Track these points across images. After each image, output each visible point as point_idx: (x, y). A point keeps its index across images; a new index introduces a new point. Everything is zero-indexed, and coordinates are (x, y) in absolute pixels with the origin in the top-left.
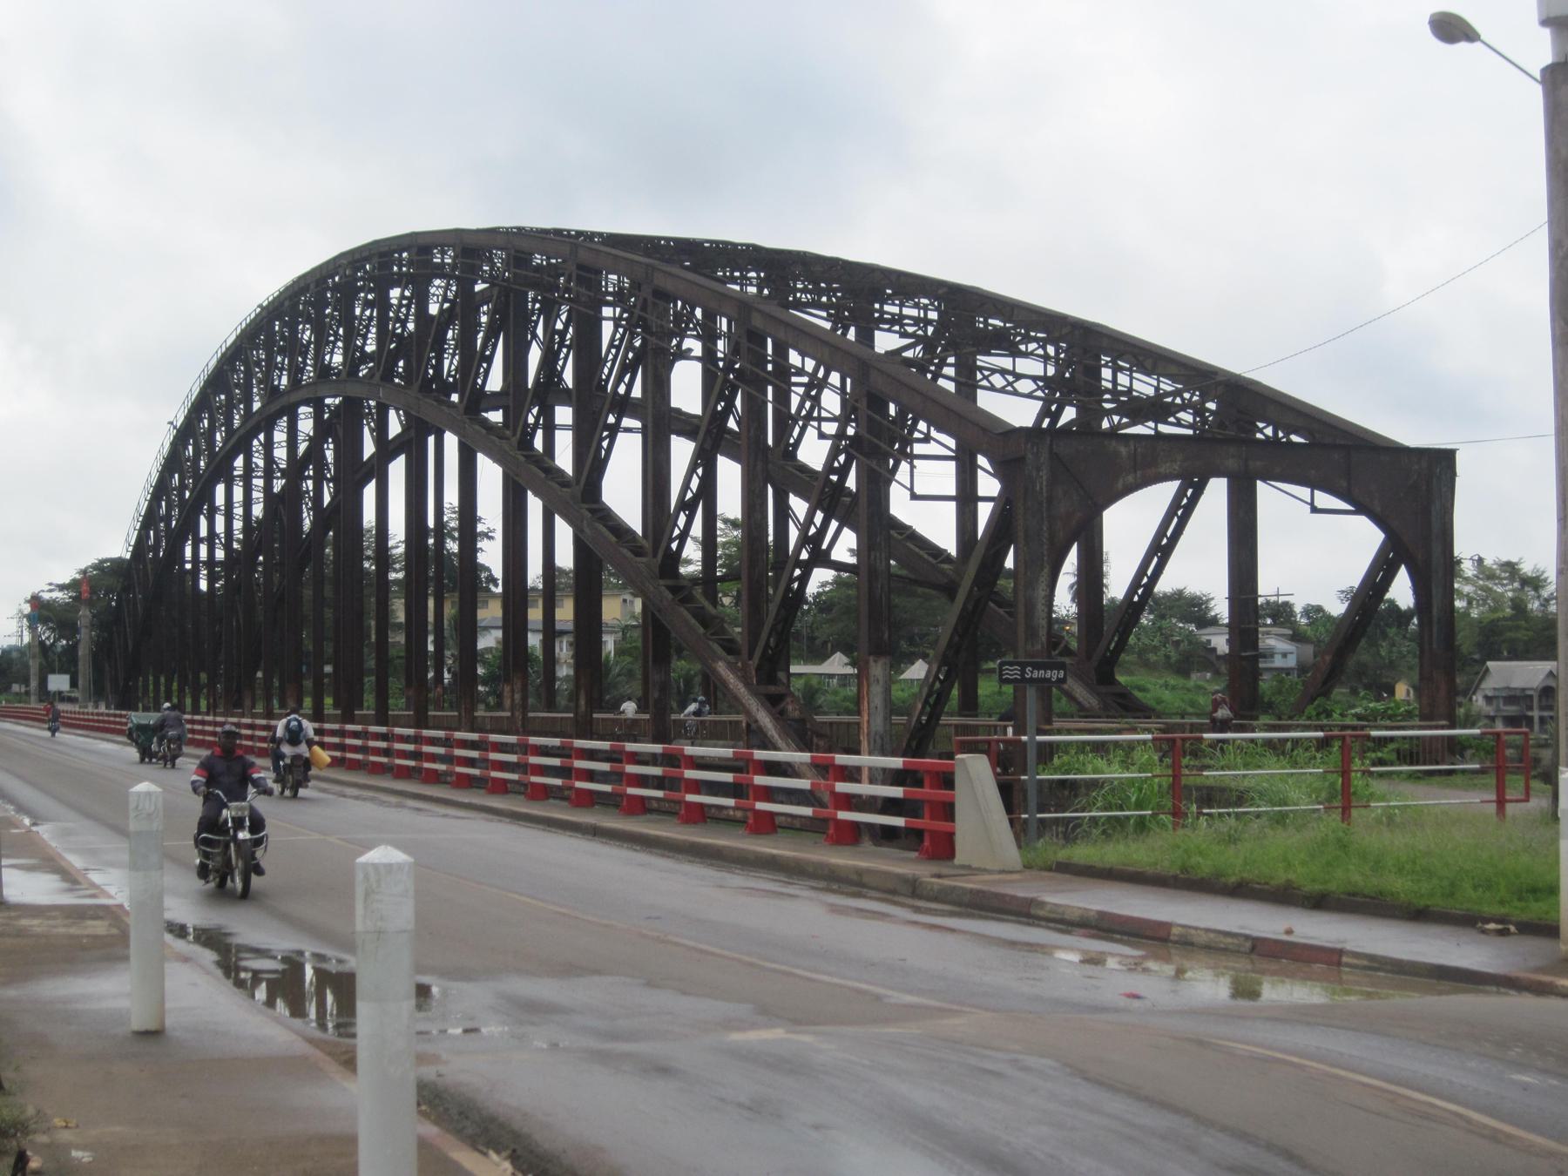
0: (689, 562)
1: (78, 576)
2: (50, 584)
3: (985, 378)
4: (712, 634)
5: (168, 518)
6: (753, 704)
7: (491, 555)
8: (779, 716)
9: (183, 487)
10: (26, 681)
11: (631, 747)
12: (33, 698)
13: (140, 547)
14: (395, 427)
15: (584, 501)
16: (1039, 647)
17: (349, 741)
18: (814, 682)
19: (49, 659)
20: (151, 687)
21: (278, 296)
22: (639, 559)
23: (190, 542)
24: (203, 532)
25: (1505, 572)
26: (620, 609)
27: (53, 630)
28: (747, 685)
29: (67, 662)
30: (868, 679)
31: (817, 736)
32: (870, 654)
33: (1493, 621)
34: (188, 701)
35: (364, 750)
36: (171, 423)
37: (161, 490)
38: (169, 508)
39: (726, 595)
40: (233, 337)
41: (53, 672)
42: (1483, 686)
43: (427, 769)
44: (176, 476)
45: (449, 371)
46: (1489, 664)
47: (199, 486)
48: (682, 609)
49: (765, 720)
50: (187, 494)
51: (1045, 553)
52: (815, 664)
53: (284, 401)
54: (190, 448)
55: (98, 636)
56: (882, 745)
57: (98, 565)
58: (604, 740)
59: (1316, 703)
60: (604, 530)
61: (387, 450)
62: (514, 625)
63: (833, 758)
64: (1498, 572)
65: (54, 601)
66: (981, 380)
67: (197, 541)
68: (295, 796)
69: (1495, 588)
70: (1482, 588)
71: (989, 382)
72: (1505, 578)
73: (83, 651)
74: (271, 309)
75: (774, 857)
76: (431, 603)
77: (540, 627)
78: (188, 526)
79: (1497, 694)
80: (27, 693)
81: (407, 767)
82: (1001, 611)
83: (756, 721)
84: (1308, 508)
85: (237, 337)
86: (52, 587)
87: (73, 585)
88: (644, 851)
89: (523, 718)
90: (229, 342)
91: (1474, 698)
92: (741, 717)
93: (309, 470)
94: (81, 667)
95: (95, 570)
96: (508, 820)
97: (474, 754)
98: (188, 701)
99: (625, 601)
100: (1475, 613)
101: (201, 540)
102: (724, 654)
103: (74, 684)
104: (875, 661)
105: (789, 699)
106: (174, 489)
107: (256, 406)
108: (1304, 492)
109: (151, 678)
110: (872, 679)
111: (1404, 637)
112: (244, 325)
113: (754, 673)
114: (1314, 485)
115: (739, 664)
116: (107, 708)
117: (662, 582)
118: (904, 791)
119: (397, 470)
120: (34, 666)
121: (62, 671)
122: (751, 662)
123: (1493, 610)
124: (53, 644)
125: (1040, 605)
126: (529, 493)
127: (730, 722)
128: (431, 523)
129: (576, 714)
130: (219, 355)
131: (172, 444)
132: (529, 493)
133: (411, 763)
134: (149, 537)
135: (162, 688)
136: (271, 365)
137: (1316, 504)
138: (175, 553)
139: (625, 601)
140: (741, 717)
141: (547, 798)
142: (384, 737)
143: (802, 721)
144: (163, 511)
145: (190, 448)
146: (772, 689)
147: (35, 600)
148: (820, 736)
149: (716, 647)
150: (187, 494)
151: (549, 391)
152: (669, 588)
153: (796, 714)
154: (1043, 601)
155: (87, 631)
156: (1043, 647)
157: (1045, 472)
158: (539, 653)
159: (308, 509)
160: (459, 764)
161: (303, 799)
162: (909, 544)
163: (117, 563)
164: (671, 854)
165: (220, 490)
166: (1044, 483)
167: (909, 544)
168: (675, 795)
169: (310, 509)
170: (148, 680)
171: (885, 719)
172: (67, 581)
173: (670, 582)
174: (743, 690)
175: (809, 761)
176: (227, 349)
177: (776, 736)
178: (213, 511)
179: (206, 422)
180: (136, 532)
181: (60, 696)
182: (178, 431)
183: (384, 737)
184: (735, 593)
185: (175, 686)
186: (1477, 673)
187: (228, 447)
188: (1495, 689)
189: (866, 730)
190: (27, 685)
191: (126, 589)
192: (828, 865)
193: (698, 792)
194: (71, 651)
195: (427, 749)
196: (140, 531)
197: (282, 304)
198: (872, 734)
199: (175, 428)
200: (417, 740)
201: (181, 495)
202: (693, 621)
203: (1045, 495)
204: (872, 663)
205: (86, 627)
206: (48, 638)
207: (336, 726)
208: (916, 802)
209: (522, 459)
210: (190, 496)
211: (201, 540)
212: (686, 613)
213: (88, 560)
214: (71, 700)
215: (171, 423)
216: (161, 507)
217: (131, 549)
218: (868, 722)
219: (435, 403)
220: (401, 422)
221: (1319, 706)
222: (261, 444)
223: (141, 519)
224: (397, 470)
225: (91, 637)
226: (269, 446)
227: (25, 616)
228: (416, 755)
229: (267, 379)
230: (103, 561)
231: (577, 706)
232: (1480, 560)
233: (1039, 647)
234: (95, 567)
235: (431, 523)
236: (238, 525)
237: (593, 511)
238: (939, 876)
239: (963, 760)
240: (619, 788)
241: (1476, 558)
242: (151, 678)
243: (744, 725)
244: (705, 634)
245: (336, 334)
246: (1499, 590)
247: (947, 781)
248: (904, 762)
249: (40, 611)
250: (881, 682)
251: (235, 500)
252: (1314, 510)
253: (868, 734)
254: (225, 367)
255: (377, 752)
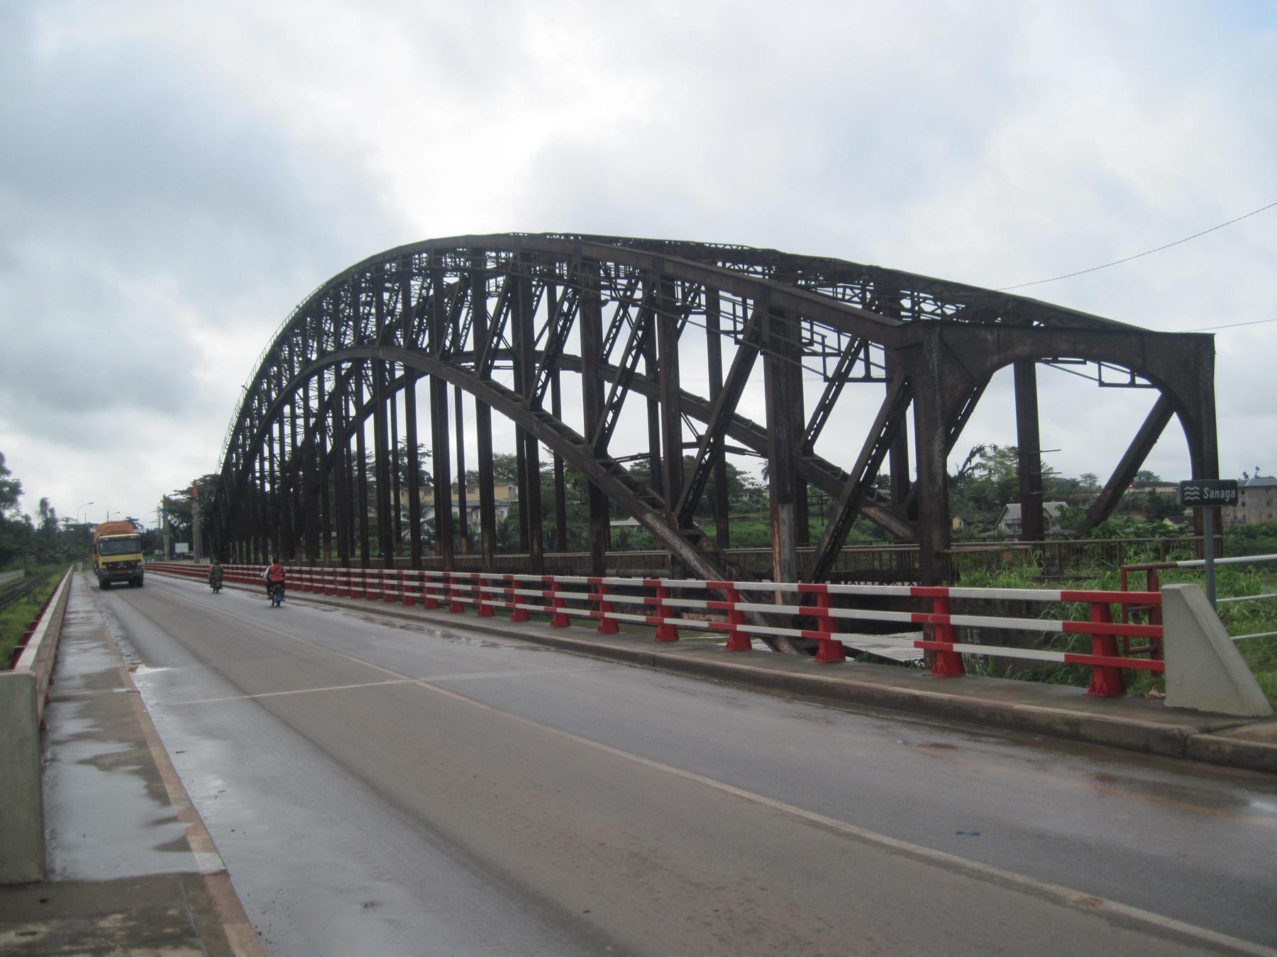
0: (545, 464)
1: (191, 486)
2: (175, 491)
3: (856, 295)
4: (640, 495)
5: (243, 446)
6: (677, 543)
7: (428, 466)
8: (700, 552)
9: (252, 426)
10: (162, 548)
11: (483, 575)
12: (166, 558)
13: (227, 465)
14: (367, 397)
15: (531, 410)
16: (937, 490)
17: (315, 577)
18: (626, 530)
19: (174, 534)
20: (237, 548)
21: (309, 301)
22: (578, 446)
23: (258, 460)
24: (266, 454)
25: (1012, 453)
26: (505, 494)
27: (178, 517)
28: (672, 528)
29: (186, 536)
30: (778, 521)
31: (729, 564)
32: (779, 502)
33: (1006, 481)
34: (261, 557)
35: (311, 580)
36: (244, 386)
37: (239, 429)
38: (244, 439)
39: (567, 483)
40: (281, 329)
41: (178, 542)
42: (1005, 518)
43: (354, 591)
44: (248, 420)
45: (424, 334)
46: (1007, 505)
47: (263, 424)
48: (615, 479)
49: (687, 553)
50: (255, 430)
51: (939, 416)
52: (622, 520)
53: (315, 366)
54: (256, 402)
55: (205, 520)
56: (790, 569)
57: (204, 479)
58: (499, 573)
59: (1100, 526)
60: (549, 428)
61: (363, 412)
62: (442, 504)
63: (601, 580)
64: (1008, 453)
65: (178, 500)
66: (859, 293)
67: (262, 460)
68: (278, 605)
69: (1006, 462)
70: (999, 463)
71: (854, 292)
72: (1012, 457)
73: (195, 529)
74: (305, 308)
75: (916, 698)
76: (392, 495)
77: (458, 504)
78: (257, 449)
79: (1014, 522)
80: (163, 555)
81: (393, 595)
82: (828, 473)
83: (681, 555)
84: (1097, 383)
85: (284, 329)
86: (177, 493)
87: (189, 491)
88: (797, 699)
89: (490, 560)
90: (278, 333)
91: (1000, 525)
92: (666, 552)
93: (329, 413)
94: (194, 538)
95: (201, 481)
96: (554, 649)
97: (395, 582)
98: (261, 557)
99: (510, 488)
100: (994, 479)
101: (265, 459)
102: (651, 508)
103: (191, 548)
104: (782, 508)
105: (704, 539)
106: (247, 428)
107: (297, 371)
108: (1091, 368)
109: (237, 543)
110: (780, 521)
111: (954, 493)
112: (287, 321)
113: (676, 521)
114: (1098, 359)
115: (664, 515)
116: (1151, 623)
117: (597, 461)
118: (589, 596)
119: (369, 424)
120: (166, 539)
121: (183, 541)
122: (674, 513)
123: (1007, 474)
124: (178, 526)
125: (936, 457)
126: (492, 408)
127: (579, 557)
128: (390, 448)
129: (532, 555)
130: (284, 325)
131: (253, 383)
132: (492, 408)
133: (361, 589)
134: (232, 458)
135: (245, 549)
136: (306, 346)
137: (1103, 380)
138: (249, 467)
139: (510, 488)
140: (666, 552)
141: (493, 615)
142: (343, 574)
143: (717, 554)
144: (241, 441)
145: (256, 402)
146: (690, 531)
147: (166, 501)
148: (731, 564)
149: (644, 504)
150: (255, 430)
151: (555, 360)
152: (602, 464)
153: (711, 549)
154: (939, 454)
155: (198, 516)
156: (940, 490)
157: (936, 354)
158: (632, 463)
159: (329, 437)
160: (354, 586)
161: (283, 607)
162: (753, 431)
163: (214, 477)
164: (759, 688)
165: (276, 427)
166: (935, 363)
167: (753, 431)
168: (511, 604)
169: (331, 437)
170: (235, 544)
171: (791, 550)
172: (185, 489)
173: (602, 461)
174: (668, 533)
175: (796, 589)
176: (277, 338)
177: (698, 566)
178: (271, 440)
179: (265, 385)
180: (221, 469)
181: (183, 556)
182: (248, 391)
183: (343, 574)
184: (573, 481)
185: (252, 547)
186: (1001, 511)
187: (280, 398)
188: (1013, 520)
189: (777, 559)
190: (163, 551)
191: (220, 490)
192: (1012, 712)
193: (564, 606)
194: (189, 528)
195: (369, 580)
196: (227, 454)
197: (312, 305)
198: (782, 562)
199: (246, 389)
200: (363, 575)
201: (251, 431)
202: (624, 487)
203: (936, 371)
204: (780, 509)
205: (196, 514)
206: (175, 522)
207: (308, 569)
208: (808, 617)
209: (485, 386)
210: (257, 432)
211: (265, 459)
212: (618, 481)
213: (198, 475)
214: (189, 558)
215: (244, 386)
216: (239, 439)
217: (222, 465)
218: (779, 552)
219: (419, 356)
220: (370, 393)
221: (1102, 527)
222: (301, 398)
223: (227, 447)
224: (369, 424)
225: (200, 521)
226: (306, 399)
227: (161, 510)
228: (364, 585)
229: (304, 354)
230: (206, 476)
231: (532, 549)
232: (995, 447)
233: (937, 490)
234: (201, 480)
235: (390, 448)
236: (288, 449)
237: (539, 416)
238: (1208, 731)
239: (1177, 592)
240: (477, 601)
241: (993, 446)
242: (237, 543)
243: (669, 558)
244: (635, 495)
245: (347, 326)
246: (1009, 463)
247: (1153, 609)
248: (588, 579)
249: (169, 506)
250: (787, 522)
251: (285, 433)
252: (1102, 384)
253: (780, 562)
254: (288, 334)
255: (357, 584)
